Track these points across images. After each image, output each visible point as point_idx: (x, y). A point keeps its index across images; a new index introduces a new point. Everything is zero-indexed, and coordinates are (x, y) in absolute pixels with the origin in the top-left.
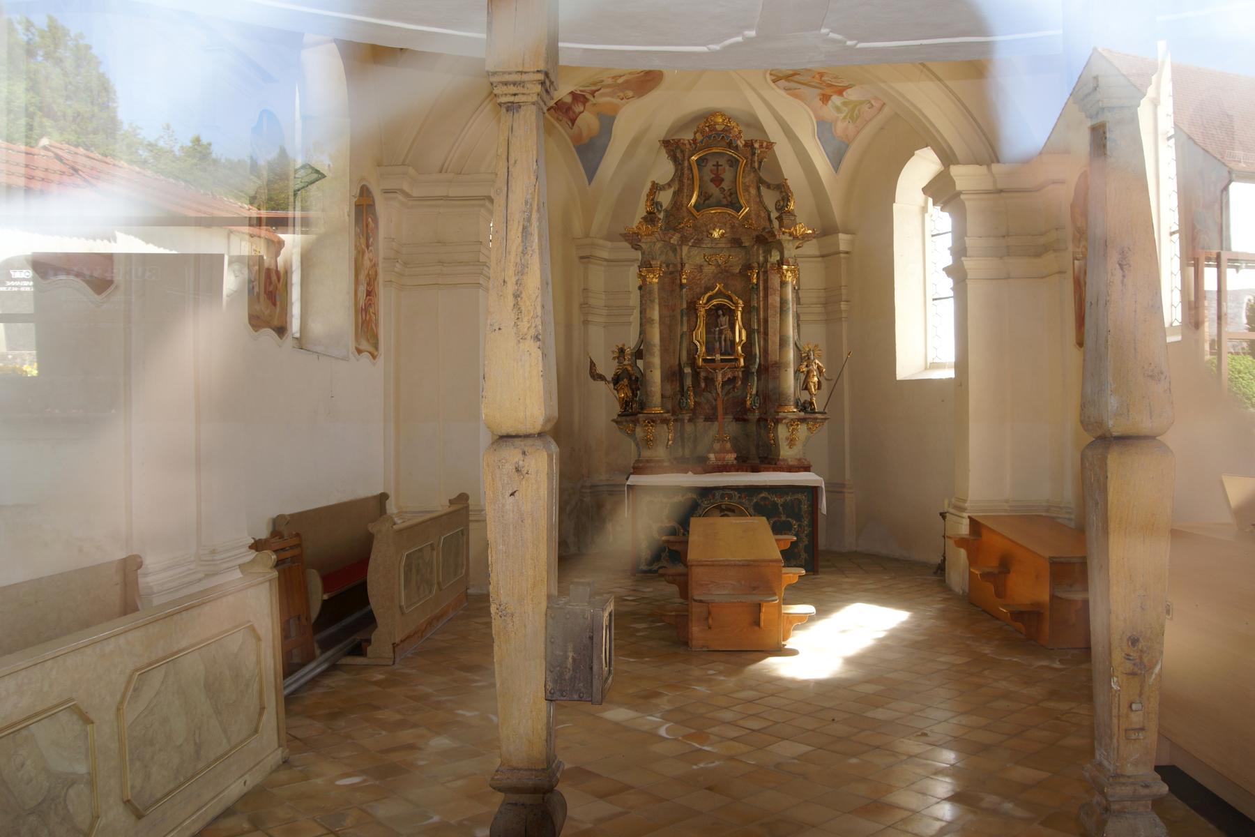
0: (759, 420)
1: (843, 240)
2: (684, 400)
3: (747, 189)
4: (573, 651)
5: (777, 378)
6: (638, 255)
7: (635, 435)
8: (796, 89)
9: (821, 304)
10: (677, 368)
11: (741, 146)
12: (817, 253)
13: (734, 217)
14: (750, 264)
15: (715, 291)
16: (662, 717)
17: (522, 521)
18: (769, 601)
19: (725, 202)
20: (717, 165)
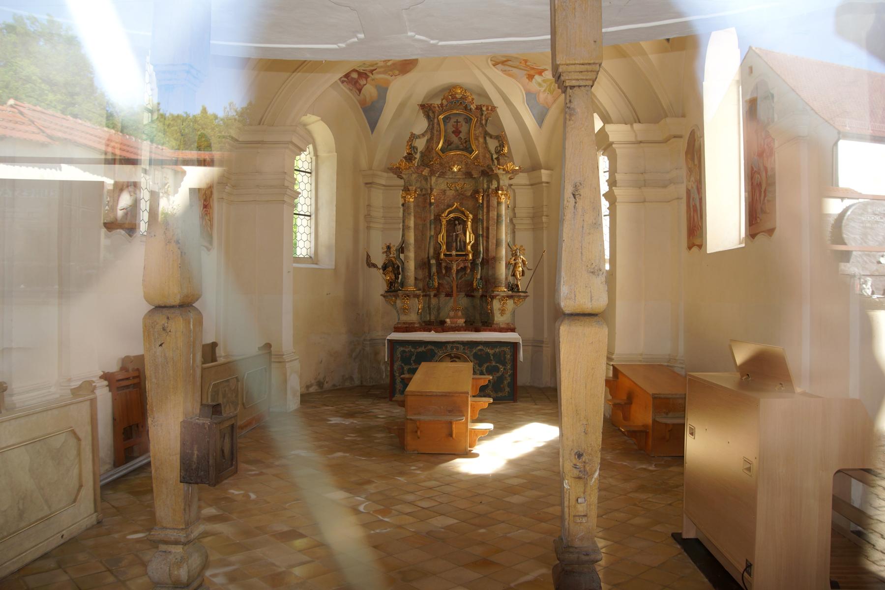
0: (482, 296)
1: (545, 174)
2: (431, 282)
3: (477, 139)
4: (198, 450)
5: (494, 268)
6: (401, 182)
7: (396, 305)
8: (509, 71)
9: (530, 218)
10: (426, 260)
11: (474, 109)
12: (528, 183)
13: (468, 157)
14: (478, 190)
15: (453, 208)
16: (365, 498)
17: (167, 363)
18: (457, 420)
19: (461, 147)
20: (457, 122)
